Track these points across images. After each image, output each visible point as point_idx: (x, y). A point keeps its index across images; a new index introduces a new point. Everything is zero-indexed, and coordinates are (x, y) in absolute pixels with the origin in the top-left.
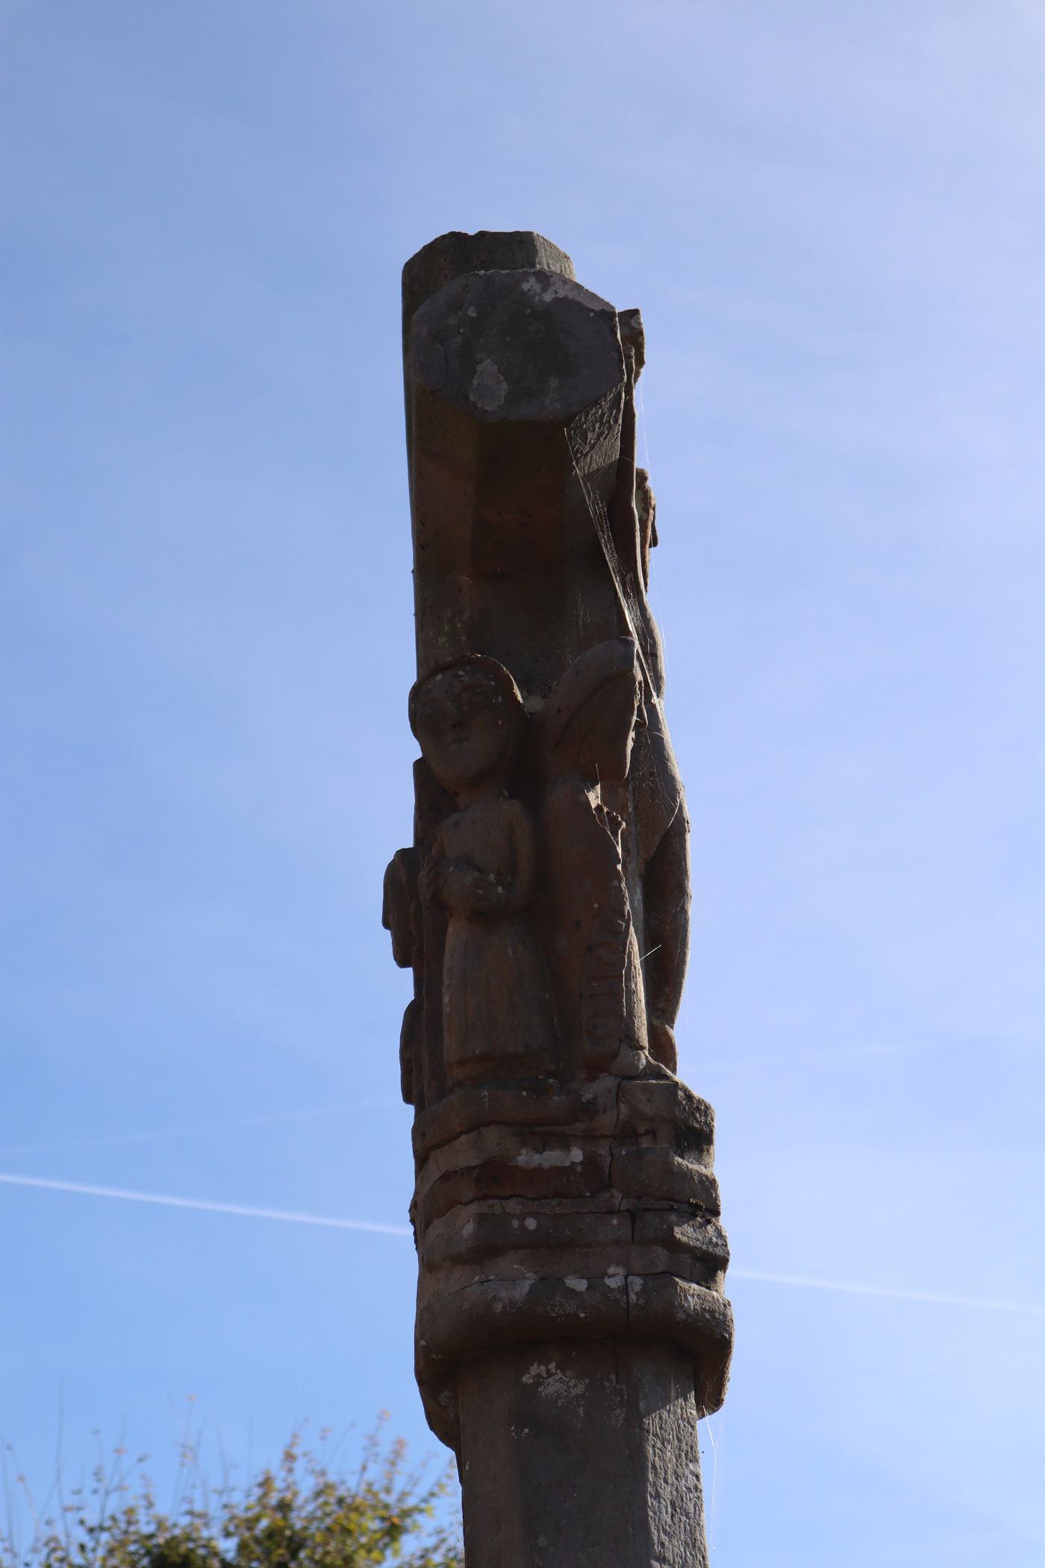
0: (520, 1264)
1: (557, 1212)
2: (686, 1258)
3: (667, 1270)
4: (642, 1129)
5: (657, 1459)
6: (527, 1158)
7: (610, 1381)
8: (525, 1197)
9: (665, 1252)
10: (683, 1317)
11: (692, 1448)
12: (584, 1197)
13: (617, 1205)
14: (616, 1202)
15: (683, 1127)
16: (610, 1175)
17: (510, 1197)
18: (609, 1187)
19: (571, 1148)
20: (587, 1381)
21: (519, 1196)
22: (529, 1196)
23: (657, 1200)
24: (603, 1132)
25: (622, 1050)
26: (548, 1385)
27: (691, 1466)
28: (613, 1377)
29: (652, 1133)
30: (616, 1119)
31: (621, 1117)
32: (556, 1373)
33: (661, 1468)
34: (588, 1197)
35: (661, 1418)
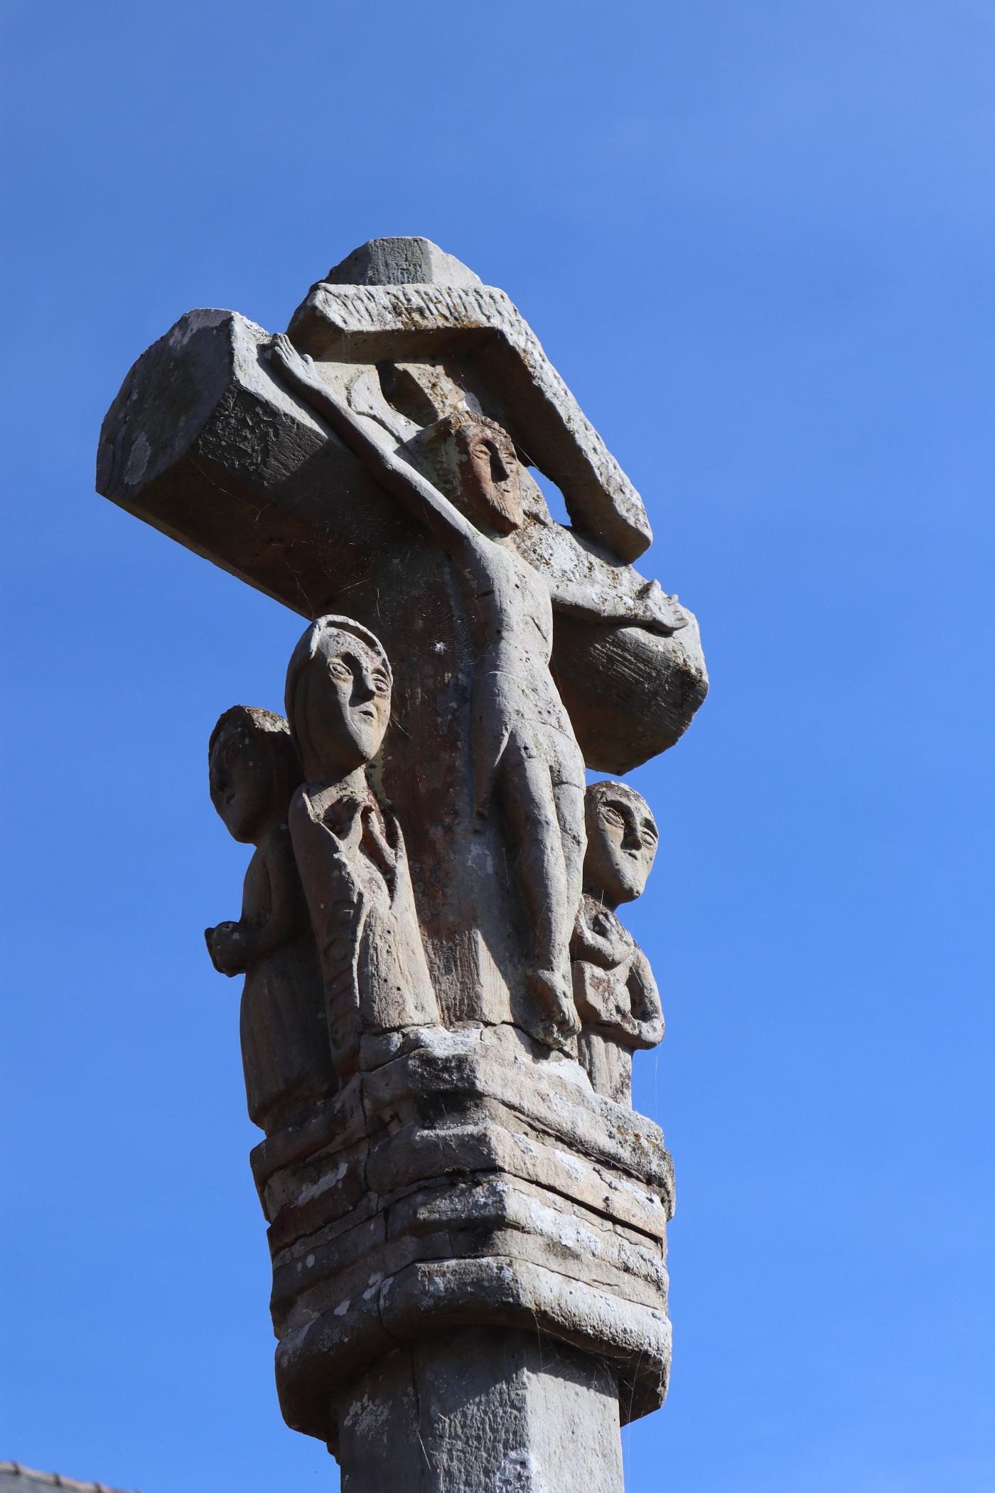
0: (308, 1307)
1: (330, 1238)
2: (443, 1236)
3: (417, 1258)
4: (387, 1117)
5: (455, 1462)
6: (310, 1192)
7: (407, 1395)
8: (304, 1235)
9: (414, 1239)
10: (431, 1302)
11: (515, 1433)
12: (350, 1212)
13: (375, 1208)
14: (373, 1205)
15: (425, 1097)
16: (366, 1178)
17: (294, 1243)
18: (364, 1193)
19: (339, 1165)
20: (391, 1403)
21: (302, 1236)
22: (308, 1233)
23: (408, 1186)
24: (358, 1137)
25: (363, 1043)
26: (362, 1421)
27: (513, 1454)
28: (410, 1390)
29: (395, 1116)
30: (363, 1118)
31: (367, 1113)
32: (368, 1406)
33: (460, 1472)
34: (352, 1210)
35: (464, 1415)
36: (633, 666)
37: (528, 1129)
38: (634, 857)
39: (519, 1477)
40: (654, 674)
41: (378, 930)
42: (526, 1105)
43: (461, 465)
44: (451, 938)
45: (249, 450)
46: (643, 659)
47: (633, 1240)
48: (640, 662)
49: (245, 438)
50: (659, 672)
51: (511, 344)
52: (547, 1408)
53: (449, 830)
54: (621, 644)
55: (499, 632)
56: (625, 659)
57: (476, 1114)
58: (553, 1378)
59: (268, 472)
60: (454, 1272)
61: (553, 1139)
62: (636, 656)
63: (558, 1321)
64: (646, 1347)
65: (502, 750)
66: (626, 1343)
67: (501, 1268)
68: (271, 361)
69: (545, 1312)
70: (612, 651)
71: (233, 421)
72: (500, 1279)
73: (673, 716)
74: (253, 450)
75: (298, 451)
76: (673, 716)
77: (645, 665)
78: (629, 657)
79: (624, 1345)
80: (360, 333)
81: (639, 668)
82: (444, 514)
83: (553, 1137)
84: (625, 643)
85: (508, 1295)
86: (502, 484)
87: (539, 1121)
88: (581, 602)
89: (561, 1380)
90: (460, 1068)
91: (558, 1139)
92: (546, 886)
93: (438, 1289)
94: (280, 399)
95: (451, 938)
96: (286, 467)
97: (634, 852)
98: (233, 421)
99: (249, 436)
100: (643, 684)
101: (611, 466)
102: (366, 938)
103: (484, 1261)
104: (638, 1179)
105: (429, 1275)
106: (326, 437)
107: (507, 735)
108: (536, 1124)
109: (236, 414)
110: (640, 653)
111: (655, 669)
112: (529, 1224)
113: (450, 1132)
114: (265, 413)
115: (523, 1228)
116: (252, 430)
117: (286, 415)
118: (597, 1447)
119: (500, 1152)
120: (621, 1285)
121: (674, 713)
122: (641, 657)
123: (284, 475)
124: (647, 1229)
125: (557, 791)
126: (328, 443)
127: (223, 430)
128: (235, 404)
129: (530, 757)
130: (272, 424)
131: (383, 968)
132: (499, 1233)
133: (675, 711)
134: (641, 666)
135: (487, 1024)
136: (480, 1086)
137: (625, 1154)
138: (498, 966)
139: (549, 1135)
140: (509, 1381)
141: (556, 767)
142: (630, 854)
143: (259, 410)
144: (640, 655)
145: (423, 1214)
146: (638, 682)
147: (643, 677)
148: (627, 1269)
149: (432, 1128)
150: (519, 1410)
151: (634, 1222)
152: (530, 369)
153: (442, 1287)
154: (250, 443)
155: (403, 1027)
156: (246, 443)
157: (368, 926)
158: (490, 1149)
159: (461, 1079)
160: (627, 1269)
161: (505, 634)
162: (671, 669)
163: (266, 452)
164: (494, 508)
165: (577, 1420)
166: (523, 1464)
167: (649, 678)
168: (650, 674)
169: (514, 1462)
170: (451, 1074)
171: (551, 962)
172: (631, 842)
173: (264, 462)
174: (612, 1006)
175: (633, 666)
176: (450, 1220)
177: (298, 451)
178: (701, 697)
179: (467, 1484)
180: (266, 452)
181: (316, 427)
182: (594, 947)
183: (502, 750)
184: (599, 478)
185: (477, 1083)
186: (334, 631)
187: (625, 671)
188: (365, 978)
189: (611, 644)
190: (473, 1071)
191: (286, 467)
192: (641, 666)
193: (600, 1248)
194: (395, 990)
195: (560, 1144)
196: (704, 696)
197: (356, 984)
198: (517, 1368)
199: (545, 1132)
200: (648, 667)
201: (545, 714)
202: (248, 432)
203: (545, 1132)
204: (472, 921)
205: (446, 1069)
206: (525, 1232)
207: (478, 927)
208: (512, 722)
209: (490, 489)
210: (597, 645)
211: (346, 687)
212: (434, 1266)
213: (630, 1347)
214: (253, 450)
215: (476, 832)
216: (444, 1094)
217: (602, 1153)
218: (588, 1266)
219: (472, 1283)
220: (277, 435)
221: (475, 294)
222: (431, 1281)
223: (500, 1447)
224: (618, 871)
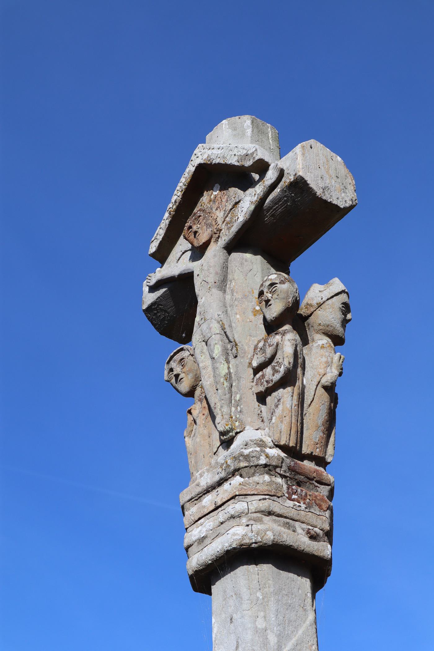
36: (279, 207)
40: (286, 199)
45: (163, 316)
46: (278, 201)
48: (279, 203)
50: (285, 196)
54: (270, 208)
56: (275, 209)
58: (220, 581)
59: (171, 314)
62: (276, 204)
63: (201, 569)
66: (221, 554)
69: (196, 571)
70: (270, 213)
73: (306, 196)
74: (164, 315)
75: (168, 301)
76: (306, 196)
77: (281, 201)
78: (275, 207)
79: (221, 555)
80: (161, 242)
81: (281, 204)
83: (203, 495)
84: (269, 207)
87: (199, 495)
91: (204, 494)
96: (172, 307)
97: (269, 303)
99: (159, 314)
100: (287, 205)
106: (164, 290)
108: (196, 498)
109: (152, 315)
110: (276, 201)
111: (284, 197)
114: (154, 306)
115: (190, 545)
116: (158, 312)
117: (157, 299)
121: (305, 195)
122: (277, 202)
123: (174, 308)
124: (229, 498)
128: (150, 314)
133: (304, 194)
137: (223, 475)
139: (201, 496)
142: (268, 306)
143: (153, 307)
144: (276, 202)
147: (285, 204)
148: (222, 523)
151: (224, 500)
156: (161, 316)
160: (222, 523)
162: (287, 190)
167: (286, 201)
168: (285, 200)
173: (168, 313)
175: (279, 207)
177: (168, 301)
178: (303, 180)
180: (166, 311)
182: (258, 365)
187: (280, 211)
189: (267, 212)
191: (172, 307)
195: (206, 495)
196: (304, 179)
199: (200, 497)
200: (282, 200)
202: (158, 314)
203: (200, 497)
206: (192, 545)
210: (266, 219)
213: (223, 554)
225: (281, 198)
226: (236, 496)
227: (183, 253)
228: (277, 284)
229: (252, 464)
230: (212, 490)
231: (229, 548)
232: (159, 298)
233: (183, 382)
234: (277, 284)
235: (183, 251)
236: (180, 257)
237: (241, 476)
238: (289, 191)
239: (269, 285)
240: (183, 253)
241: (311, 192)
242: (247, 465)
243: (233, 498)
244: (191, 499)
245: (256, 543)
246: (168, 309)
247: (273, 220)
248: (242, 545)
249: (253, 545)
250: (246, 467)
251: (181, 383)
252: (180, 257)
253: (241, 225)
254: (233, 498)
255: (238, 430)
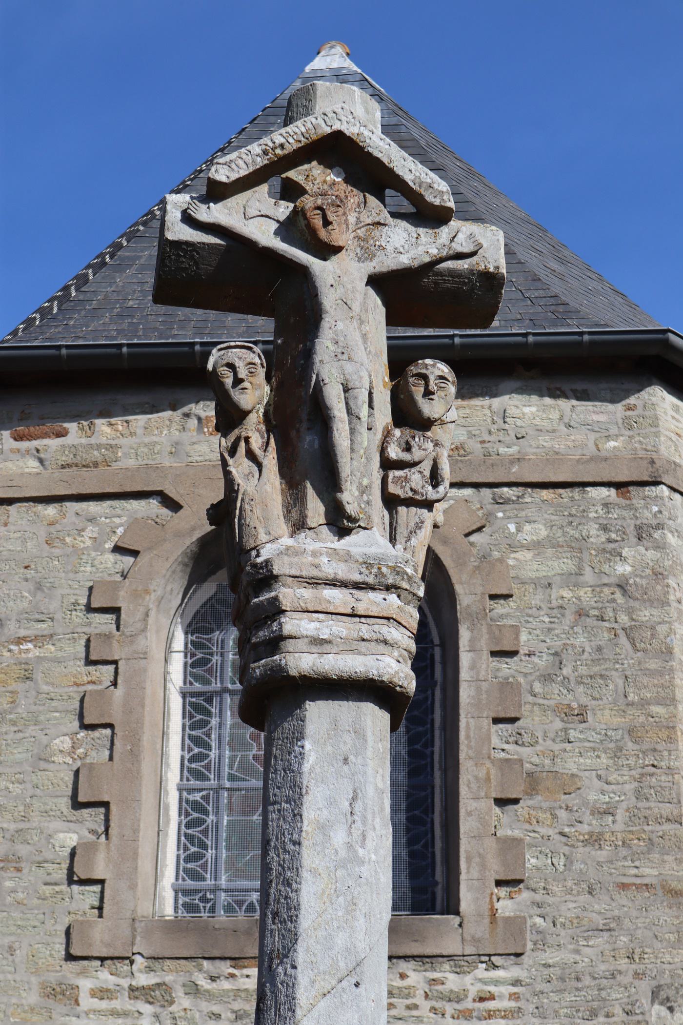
37: (306, 585)
38: (432, 399)
39: (300, 754)
41: (247, 500)
42: (304, 574)
43: (306, 226)
44: (297, 488)
47: (371, 623)
49: (183, 262)
50: (469, 278)
51: (348, 134)
52: (319, 717)
53: (298, 431)
54: (440, 274)
55: (321, 316)
56: (445, 280)
57: (276, 586)
60: (263, 666)
61: (324, 586)
64: (371, 677)
65: (312, 385)
67: (280, 660)
68: (188, 219)
71: (173, 257)
72: (280, 665)
74: (190, 265)
80: (240, 179)
82: (294, 259)
84: (441, 272)
85: (284, 672)
86: (330, 227)
88: (395, 268)
89: (330, 701)
90: (266, 566)
91: (326, 584)
92: (334, 451)
93: (257, 675)
94: (194, 236)
95: (297, 488)
96: (210, 266)
97: (431, 397)
98: (173, 257)
100: (462, 288)
101: (423, 175)
102: (241, 507)
103: (275, 658)
104: (380, 589)
105: (254, 669)
106: (222, 243)
107: (314, 376)
110: (452, 273)
112: (298, 634)
113: (264, 598)
116: (184, 257)
117: (198, 243)
118: (351, 729)
119: (284, 603)
120: (359, 648)
125: (347, 394)
126: (227, 246)
127: (170, 262)
129: (325, 384)
130: (194, 250)
131: (248, 520)
132: (283, 643)
134: (457, 280)
135: (310, 529)
136: (275, 572)
137: (371, 580)
138: (319, 496)
139: (320, 584)
140: (300, 708)
141: (345, 382)
142: (429, 399)
145: (254, 640)
146: (458, 288)
148: (363, 640)
149: (258, 597)
150: (303, 721)
151: (371, 614)
152: (361, 144)
153: (258, 673)
154: (186, 263)
155: (257, 546)
157: (242, 499)
158: (279, 602)
159: (267, 571)
160: (363, 640)
161: (323, 316)
163: (196, 264)
164: (325, 243)
165: (338, 719)
166: (303, 747)
167: (465, 283)
168: (464, 281)
169: (299, 747)
170: (263, 569)
171: (341, 488)
172: (428, 393)
173: (198, 268)
174: (407, 489)
176: (263, 641)
179: (282, 760)
180: (196, 264)
181: (218, 241)
183: (312, 385)
184: (413, 187)
185: (274, 571)
186: (222, 352)
188: (240, 526)
189: (433, 276)
190: (272, 566)
191: (210, 266)
192: (457, 280)
193: (344, 633)
194: (253, 529)
197: (237, 531)
198: (305, 701)
199: (317, 584)
201: (340, 356)
203: (317, 584)
204: (305, 477)
205: (262, 568)
207: (308, 479)
208: (317, 367)
209: (323, 234)
211: (229, 381)
212: (256, 664)
214: (190, 265)
215: (309, 429)
216: (261, 579)
217: (356, 583)
218: (336, 645)
219: (269, 670)
220: (198, 253)
221: (323, 116)
222: (255, 672)
223: (295, 740)
224: (420, 411)
225: (462, 276)
226: (393, 618)
227: (262, 216)
228: (449, 381)
229: (412, 591)
230: (340, 586)
231: (377, 678)
232: (204, 243)
233: (246, 393)
234: (449, 381)
235: (262, 213)
236: (254, 217)
237: (399, 596)
238: (478, 277)
239: (439, 376)
240: (262, 216)
241: (498, 297)
242: (408, 588)
243: (388, 619)
244: (298, 577)
245: (401, 687)
246: (203, 265)
247: (432, 287)
248: (391, 682)
249: (398, 689)
250: (406, 590)
251: (242, 393)
252: (254, 217)
253: (403, 267)
254: (388, 619)
255: (363, 525)
